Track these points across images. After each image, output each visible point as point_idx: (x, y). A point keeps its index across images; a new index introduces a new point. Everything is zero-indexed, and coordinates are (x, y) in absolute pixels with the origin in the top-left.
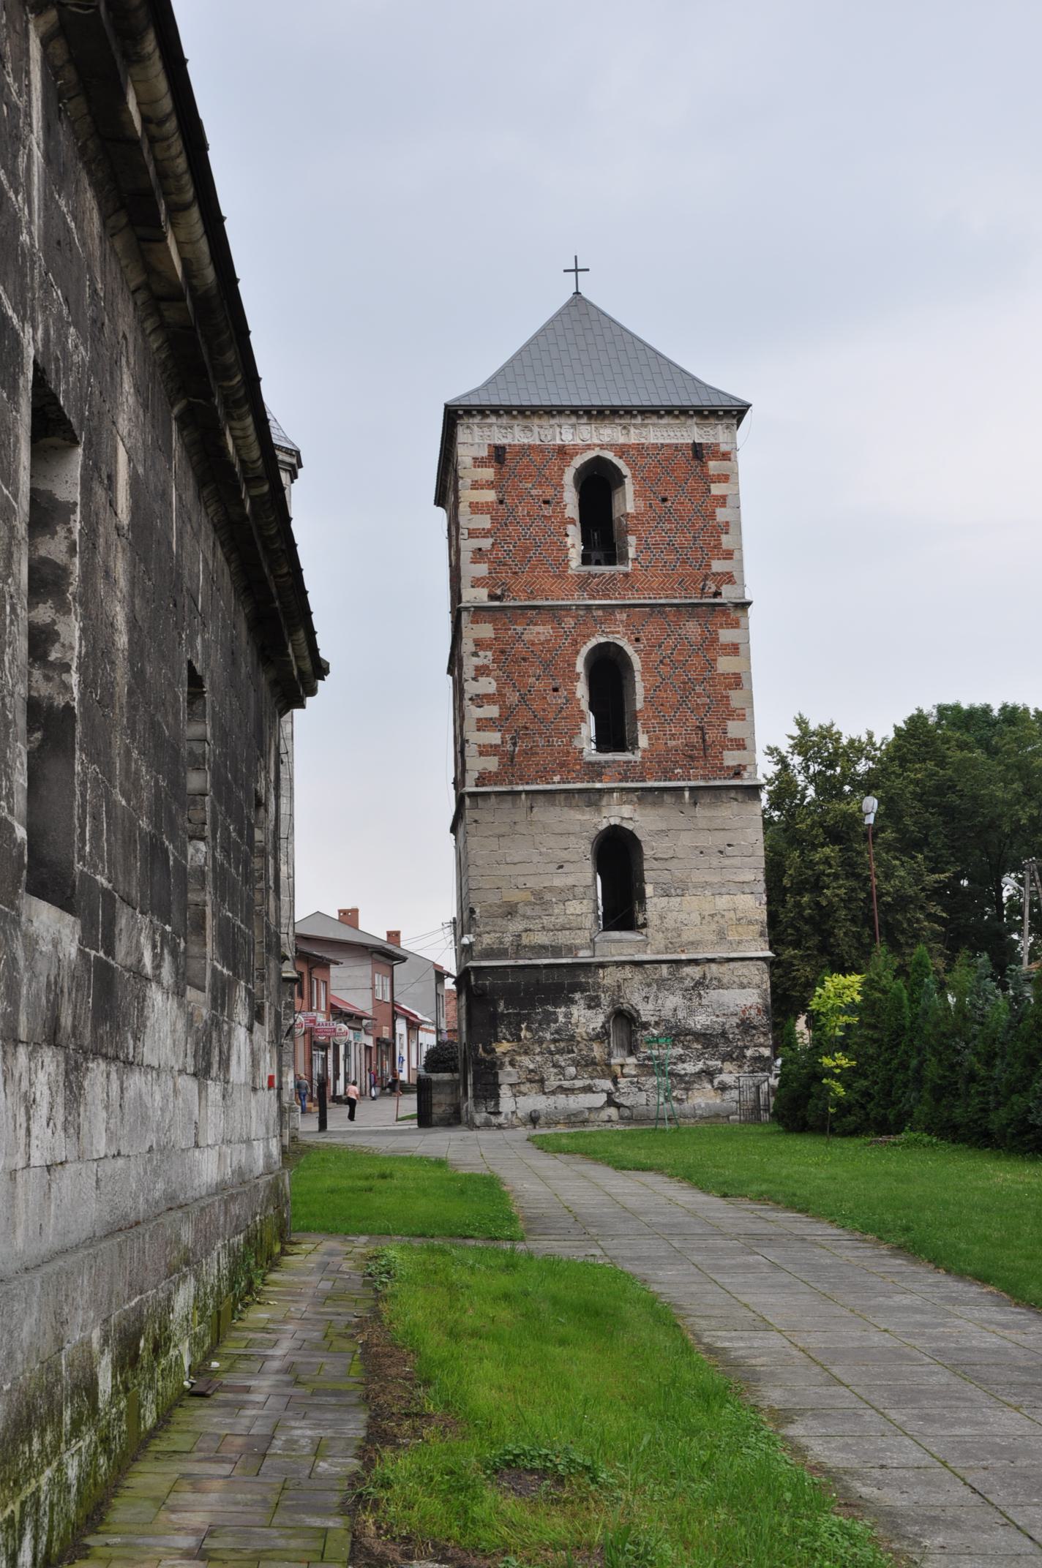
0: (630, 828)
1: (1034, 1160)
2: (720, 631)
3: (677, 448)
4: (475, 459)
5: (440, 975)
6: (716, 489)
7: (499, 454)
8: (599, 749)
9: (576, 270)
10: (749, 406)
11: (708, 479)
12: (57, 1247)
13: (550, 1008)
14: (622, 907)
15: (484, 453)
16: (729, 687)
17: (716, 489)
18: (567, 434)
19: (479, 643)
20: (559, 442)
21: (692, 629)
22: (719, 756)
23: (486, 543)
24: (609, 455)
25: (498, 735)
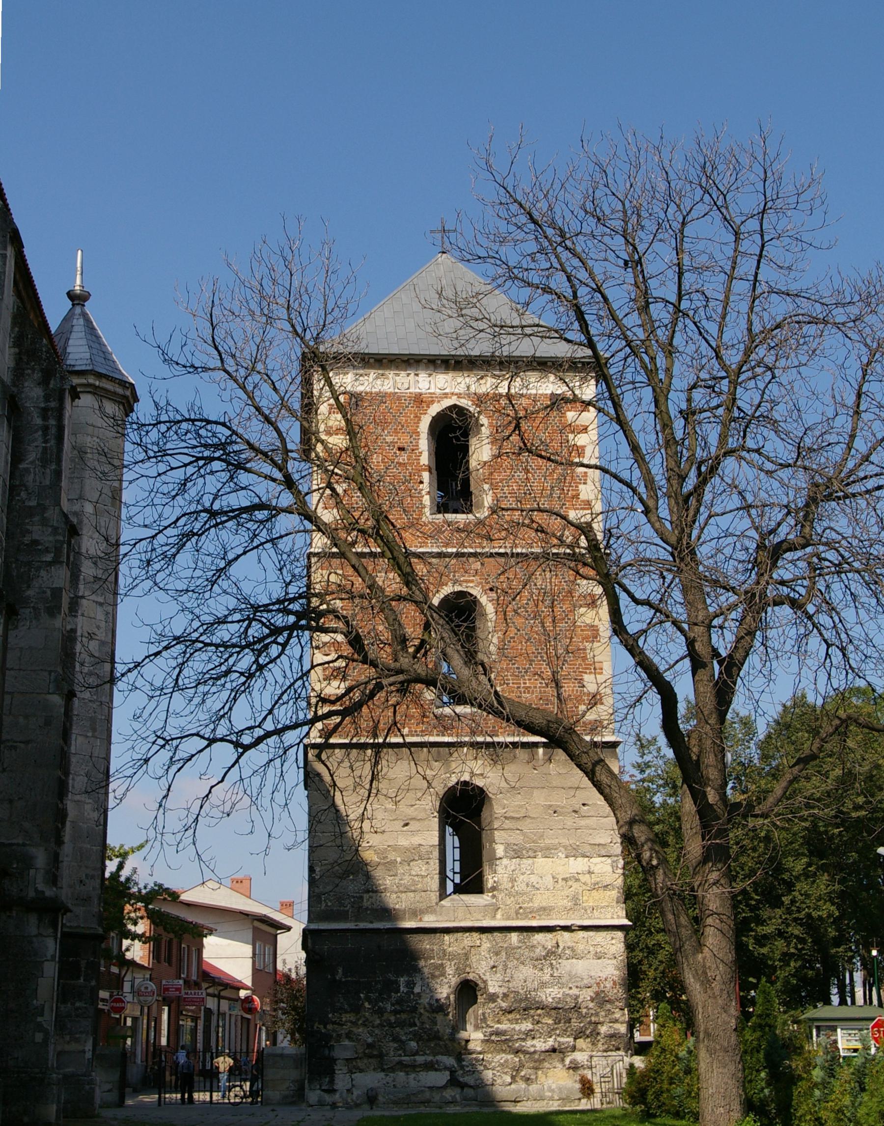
5: (83, 615)
18: (425, 382)
24: (464, 403)
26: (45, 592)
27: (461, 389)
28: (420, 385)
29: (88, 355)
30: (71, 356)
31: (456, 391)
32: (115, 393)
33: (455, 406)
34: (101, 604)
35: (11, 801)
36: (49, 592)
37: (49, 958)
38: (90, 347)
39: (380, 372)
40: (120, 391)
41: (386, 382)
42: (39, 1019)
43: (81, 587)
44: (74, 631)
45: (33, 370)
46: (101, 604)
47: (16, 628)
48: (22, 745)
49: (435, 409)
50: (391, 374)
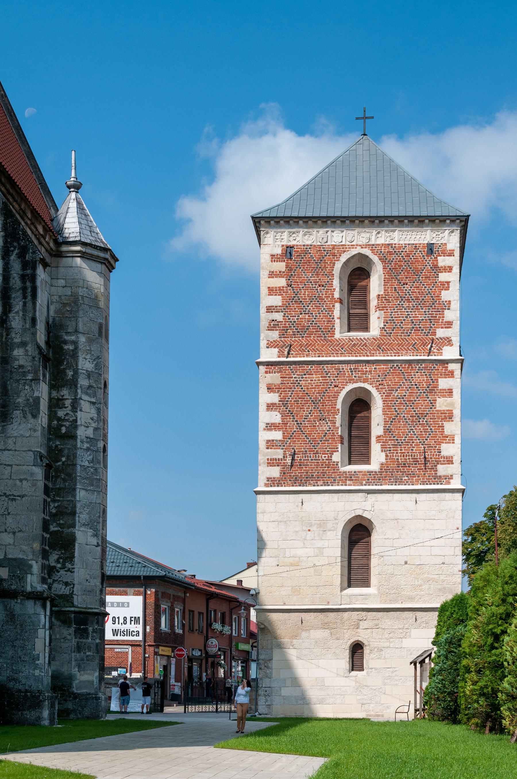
0: (369, 517)
2: (440, 380)
3: (416, 247)
4: (272, 256)
5: (81, 410)
7: (289, 251)
9: (365, 118)
10: (468, 216)
12: (321, 721)
14: (356, 569)
15: (278, 251)
18: (337, 237)
19: (450, 392)
21: (419, 378)
22: (434, 468)
23: (279, 317)
24: (367, 252)
25: (281, 452)
26: (28, 400)
27: (364, 241)
28: (334, 239)
29: (78, 230)
30: (66, 231)
31: (361, 243)
32: (98, 257)
33: (359, 254)
34: (94, 403)
35: (14, 533)
36: (31, 400)
37: (41, 627)
38: (80, 223)
39: (306, 230)
40: (102, 254)
41: (312, 237)
42: (37, 662)
43: (79, 391)
44: (76, 421)
45: (15, 248)
46: (94, 403)
47: (12, 423)
48: (19, 498)
49: (344, 258)
50: (314, 231)
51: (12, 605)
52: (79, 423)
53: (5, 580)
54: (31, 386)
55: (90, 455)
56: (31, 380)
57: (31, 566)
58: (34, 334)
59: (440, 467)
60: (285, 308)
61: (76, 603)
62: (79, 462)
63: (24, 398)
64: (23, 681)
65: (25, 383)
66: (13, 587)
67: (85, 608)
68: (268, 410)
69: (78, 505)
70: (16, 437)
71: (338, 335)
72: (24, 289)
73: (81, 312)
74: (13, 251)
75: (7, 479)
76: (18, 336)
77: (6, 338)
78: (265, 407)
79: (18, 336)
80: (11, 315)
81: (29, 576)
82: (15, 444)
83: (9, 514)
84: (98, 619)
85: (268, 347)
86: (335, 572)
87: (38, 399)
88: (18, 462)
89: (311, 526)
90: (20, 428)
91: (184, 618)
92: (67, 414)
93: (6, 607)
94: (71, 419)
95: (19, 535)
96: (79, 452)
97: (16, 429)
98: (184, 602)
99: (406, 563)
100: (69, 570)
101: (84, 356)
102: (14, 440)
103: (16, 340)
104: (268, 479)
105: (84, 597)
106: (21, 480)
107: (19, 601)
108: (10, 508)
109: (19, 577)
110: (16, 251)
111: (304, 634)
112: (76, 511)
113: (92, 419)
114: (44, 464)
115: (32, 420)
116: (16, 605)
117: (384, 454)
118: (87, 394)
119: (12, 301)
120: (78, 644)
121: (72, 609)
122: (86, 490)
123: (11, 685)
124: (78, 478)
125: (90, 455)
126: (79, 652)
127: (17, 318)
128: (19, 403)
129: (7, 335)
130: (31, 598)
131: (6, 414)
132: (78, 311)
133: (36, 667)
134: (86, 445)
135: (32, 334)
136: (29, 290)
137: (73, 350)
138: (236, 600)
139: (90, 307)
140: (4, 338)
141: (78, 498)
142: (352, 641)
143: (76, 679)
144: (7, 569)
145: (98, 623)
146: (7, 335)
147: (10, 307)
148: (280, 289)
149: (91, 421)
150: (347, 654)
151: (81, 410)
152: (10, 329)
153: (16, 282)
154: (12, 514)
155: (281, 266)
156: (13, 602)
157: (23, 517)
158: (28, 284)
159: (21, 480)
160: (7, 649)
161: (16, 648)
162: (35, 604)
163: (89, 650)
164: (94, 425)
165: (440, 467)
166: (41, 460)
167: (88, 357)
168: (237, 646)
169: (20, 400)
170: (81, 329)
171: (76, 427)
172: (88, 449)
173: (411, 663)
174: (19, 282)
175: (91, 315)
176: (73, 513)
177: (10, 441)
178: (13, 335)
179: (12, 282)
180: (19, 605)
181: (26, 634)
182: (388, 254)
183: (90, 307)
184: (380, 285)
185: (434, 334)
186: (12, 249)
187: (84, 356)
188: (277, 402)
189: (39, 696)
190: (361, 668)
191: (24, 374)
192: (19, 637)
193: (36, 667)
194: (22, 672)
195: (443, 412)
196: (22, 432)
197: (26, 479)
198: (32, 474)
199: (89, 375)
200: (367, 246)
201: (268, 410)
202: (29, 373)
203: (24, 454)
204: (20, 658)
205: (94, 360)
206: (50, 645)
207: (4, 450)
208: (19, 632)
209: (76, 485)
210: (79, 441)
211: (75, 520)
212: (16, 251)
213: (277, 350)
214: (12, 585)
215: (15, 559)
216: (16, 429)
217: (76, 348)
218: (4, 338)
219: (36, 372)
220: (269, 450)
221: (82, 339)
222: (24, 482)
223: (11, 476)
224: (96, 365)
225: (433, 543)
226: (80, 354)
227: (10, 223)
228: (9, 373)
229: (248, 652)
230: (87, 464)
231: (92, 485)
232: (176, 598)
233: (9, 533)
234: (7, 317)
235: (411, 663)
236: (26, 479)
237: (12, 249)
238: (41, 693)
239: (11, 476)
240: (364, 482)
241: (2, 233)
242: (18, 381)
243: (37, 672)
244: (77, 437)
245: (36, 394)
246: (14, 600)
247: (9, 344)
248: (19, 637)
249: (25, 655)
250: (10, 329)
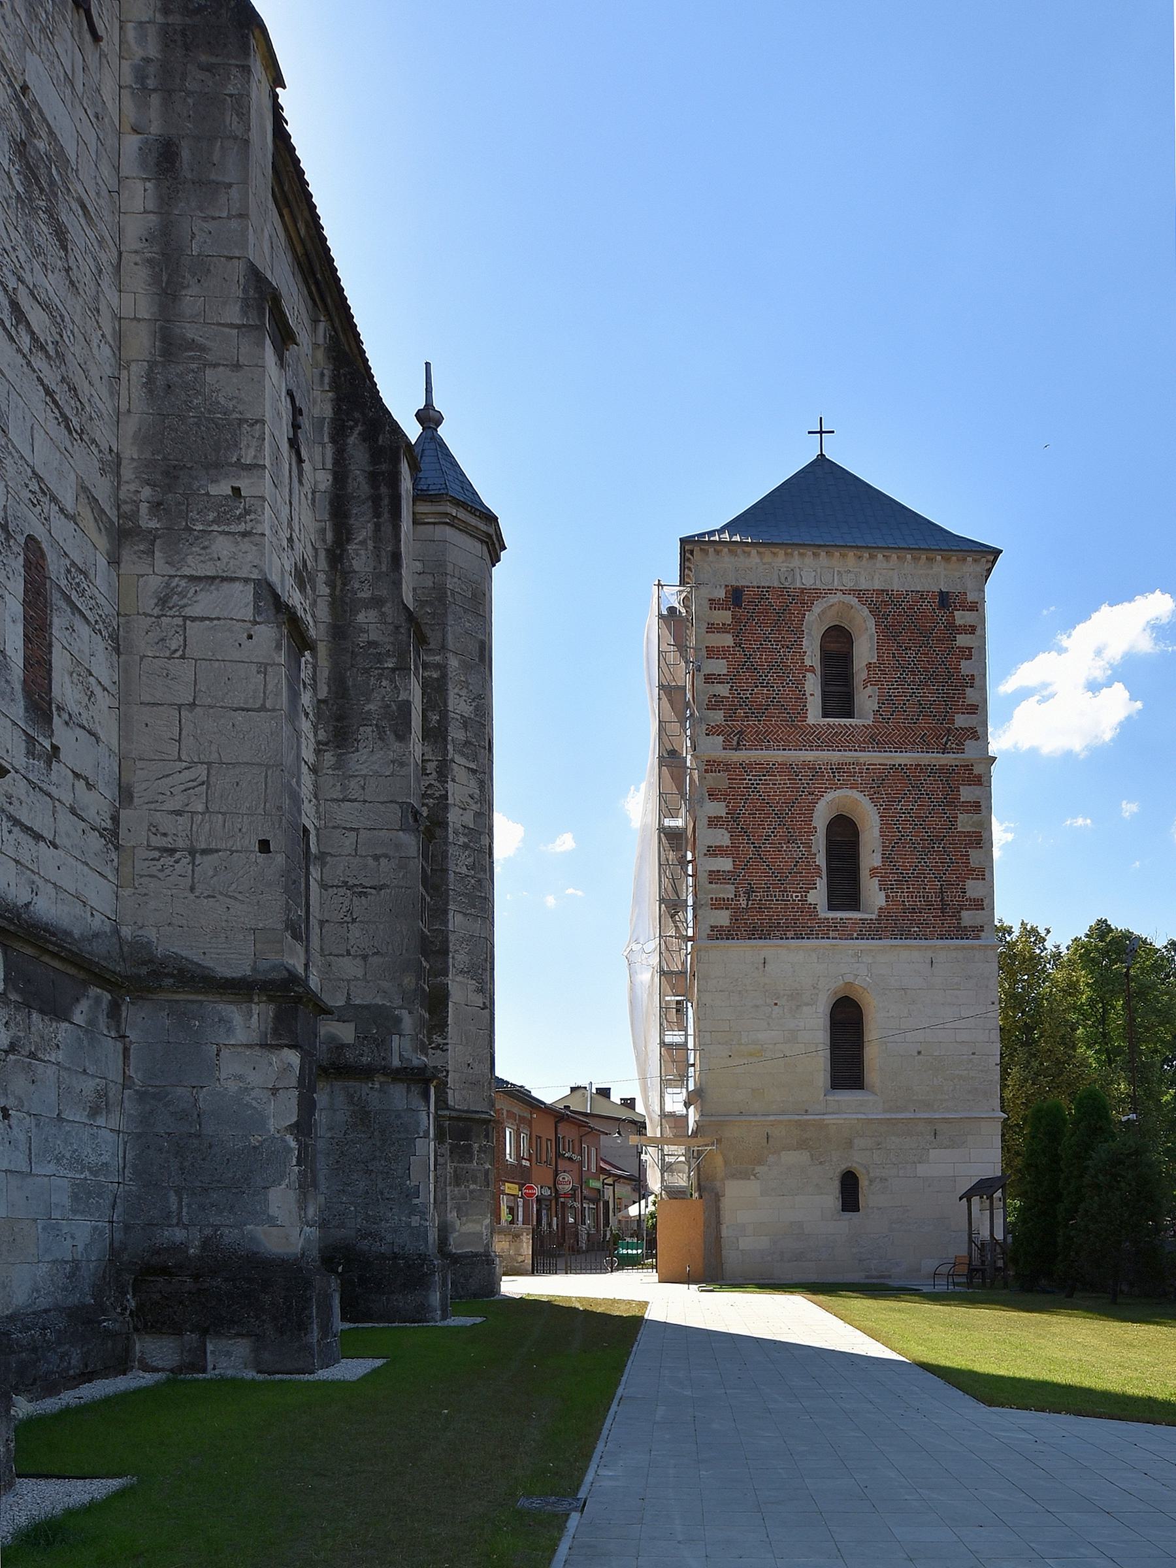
1: (1173, 1323)
3: (922, 595)
5: (453, 780)
6: (962, 640)
8: (831, 907)
9: (821, 432)
11: (954, 630)
13: (683, 810)
15: (721, 594)
16: (970, 845)
17: (962, 640)
20: (798, 585)
22: (957, 915)
25: (731, 888)
26: (389, 706)
34: (474, 771)
35: (365, 957)
36: (394, 707)
45: (356, 422)
46: (474, 771)
51: (364, 1094)
52: (450, 801)
53: (348, 1045)
54: (392, 681)
55: (469, 856)
56: (393, 670)
57: (399, 1020)
58: (397, 584)
59: (965, 914)
60: (731, 678)
61: (451, 1103)
62: (452, 866)
63: (380, 704)
64: (389, 1238)
65: (382, 675)
66: (365, 1060)
67: (467, 1111)
68: (710, 826)
69: (452, 938)
70: (365, 777)
71: (811, 720)
72: (376, 500)
73: (450, 617)
74: (352, 428)
75: (350, 855)
76: (366, 586)
77: (341, 590)
78: (705, 821)
79: (366, 586)
80: (351, 548)
81: (396, 1038)
82: (364, 789)
83: (354, 921)
84: (487, 1130)
85: (707, 735)
86: (819, 1064)
87: (407, 704)
88: (369, 824)
89: (778, 998)
90: (374, 758)
91: (530, 1146)
92: (430, 785)
93: (352, 1096)
94: (437, 794)
95: (375, 960)
96: (451, 850)
97: (366, 762)
98: (530, 1127)
99: (919, 1053)
100: (438, 1047)
101: (456, 691)
102: (362, 783)
103: (361, 595)
104: (713, 928)
105: (464, 1092)
106: (376, 858)
107: (377, 1086)
108: (356, 909)
109: (375, 1040)
110: (359, 428)
111: (772, 1159)
112: (448, 947)
113: (472, 797)
114: (422, 828)
115: (396, 745)
116: (369, 1091)
117: (883, 894)
118: (463, 755)
119: (352, 521)
120: (455, 1171)
121: (447, 1112)
122: (465, 914)
123: (364, 1245)
124: (451, 893)
125: (469, 856)
126: (458, 1185)
127: (362, 552)
128: (369, 712)
129: (344, 584)
130: (401, 1080)
131: (345, 733)
132: (445, 615)
133: (413, 1211)
134: (462, 840)
135: (394, 583)
136: (386, 501)
137: (437, 679)
138: (586, 1125)
139: (466, 611)
140: (338, 589)
141: (451, 927)
142: (843, 1167)
143: (455, 1231)
144: (352, 1026)
145: (487, 1136)
146: (344, 584)
147: (349, 532)
148: (725, 650)
149: (469, 800)
150: (836, 1184)
151: (453, 780)
152: (349, 573)
153: (359, 484)
154: (361, 922)
155: (725, 616)
156: (365, 1088)
157: (382, 927)
158: (384, 490)
159: (376, 858)
160: (355, 1177)
161: (373, 1176)
162: (409, 1090)
163: (475, 1182)
164: (475, 807)
165: (965, 914)
166: (416, 820)
167: (464, 692)
168: (587, 1182)
169: (371, 707)
170: (451, 646)
171: (446, 808)
172: (465, 846)
173: (961, 1199)
174: (366, 486)
175: (468, 624)
176: (446, 952)
177: (353, 784)
178: (356, 586)
179: (351, 486)
180: (376, 1094)
181: (392, 1149)
182: (883, 605)
183: (466, 611)
184: (871, 649)
185: (952, 721)
186: (351, 423)
187: (456, 691)
188: (724, 815)
189: (422, 1266)
190: (856, 1208)
191: (379, 658)
192: (378, 1154)
193: (413, 1211)
194: (387, 1221)
195: (968, 834)
196: (376, 767)
197: (386, 856)
198: (398, 846)
199: (465, 723)
200: (851, 591)
201: (710, 826)
202: (389, 656)
203: (382, 808)
204: (382, 1193)
205: (473, 700)
206: (435, 1169)
207: (343, 801)
208: (378, 1144)
209: (447, 904)
210: (450, 830)
211: (447, 962)
212: (359, 428)
213: (721, 738)
214: (362, 1055)
215: (367, 1007)
216: (366, 762)
217: (444, 676)
218: (338, 589)
219: (402, 655)
220: (714, 886)
221: (453, 662)
222: (383, 861)
223: (356, 850)
224: (477, 708)
225: (957, 1024)
226: (450, 687)
227: (345, 375)
228: (349, 655)
229: (599, 1190)
230: (464, 870)
231: (474, 907)
232: (522, 1119)
233: (355, 957)
234: (344, 550)
235: (961, 1199)
236: (386, 856)
237: (351, 423)
238: (425, 1260)
239: (356, 850)
240: (855, 935)
241: (330, 394)
242: (367, 671)
243: (415, 1221)
244: (447, 824)
245: (403, 696)
246: (367, 1084)
247: (348, 601)
248: (378, 1154)
249: (391, 1187)
250: (349, 573)
